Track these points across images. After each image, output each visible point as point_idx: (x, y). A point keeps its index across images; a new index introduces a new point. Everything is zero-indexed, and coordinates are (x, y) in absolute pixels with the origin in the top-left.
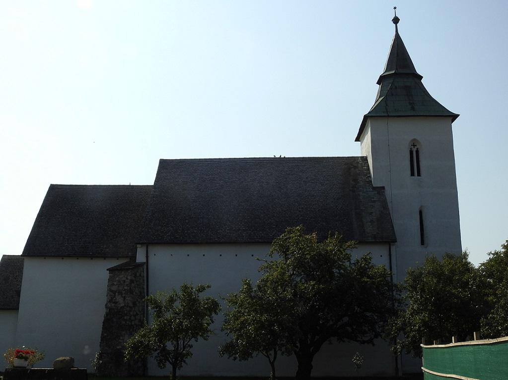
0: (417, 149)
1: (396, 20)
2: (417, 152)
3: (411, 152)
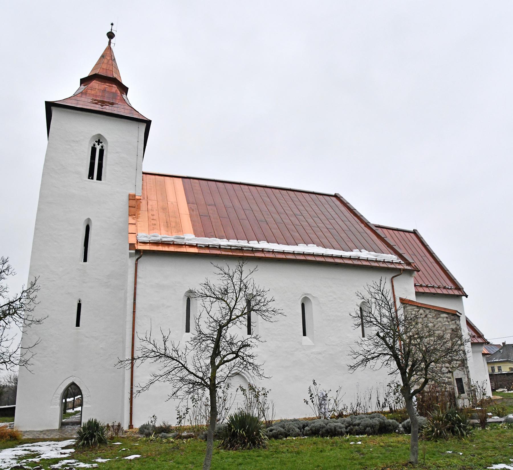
0: (102, 147)
1: (111, 35)
2: (102, 151)
3: (94, 150)
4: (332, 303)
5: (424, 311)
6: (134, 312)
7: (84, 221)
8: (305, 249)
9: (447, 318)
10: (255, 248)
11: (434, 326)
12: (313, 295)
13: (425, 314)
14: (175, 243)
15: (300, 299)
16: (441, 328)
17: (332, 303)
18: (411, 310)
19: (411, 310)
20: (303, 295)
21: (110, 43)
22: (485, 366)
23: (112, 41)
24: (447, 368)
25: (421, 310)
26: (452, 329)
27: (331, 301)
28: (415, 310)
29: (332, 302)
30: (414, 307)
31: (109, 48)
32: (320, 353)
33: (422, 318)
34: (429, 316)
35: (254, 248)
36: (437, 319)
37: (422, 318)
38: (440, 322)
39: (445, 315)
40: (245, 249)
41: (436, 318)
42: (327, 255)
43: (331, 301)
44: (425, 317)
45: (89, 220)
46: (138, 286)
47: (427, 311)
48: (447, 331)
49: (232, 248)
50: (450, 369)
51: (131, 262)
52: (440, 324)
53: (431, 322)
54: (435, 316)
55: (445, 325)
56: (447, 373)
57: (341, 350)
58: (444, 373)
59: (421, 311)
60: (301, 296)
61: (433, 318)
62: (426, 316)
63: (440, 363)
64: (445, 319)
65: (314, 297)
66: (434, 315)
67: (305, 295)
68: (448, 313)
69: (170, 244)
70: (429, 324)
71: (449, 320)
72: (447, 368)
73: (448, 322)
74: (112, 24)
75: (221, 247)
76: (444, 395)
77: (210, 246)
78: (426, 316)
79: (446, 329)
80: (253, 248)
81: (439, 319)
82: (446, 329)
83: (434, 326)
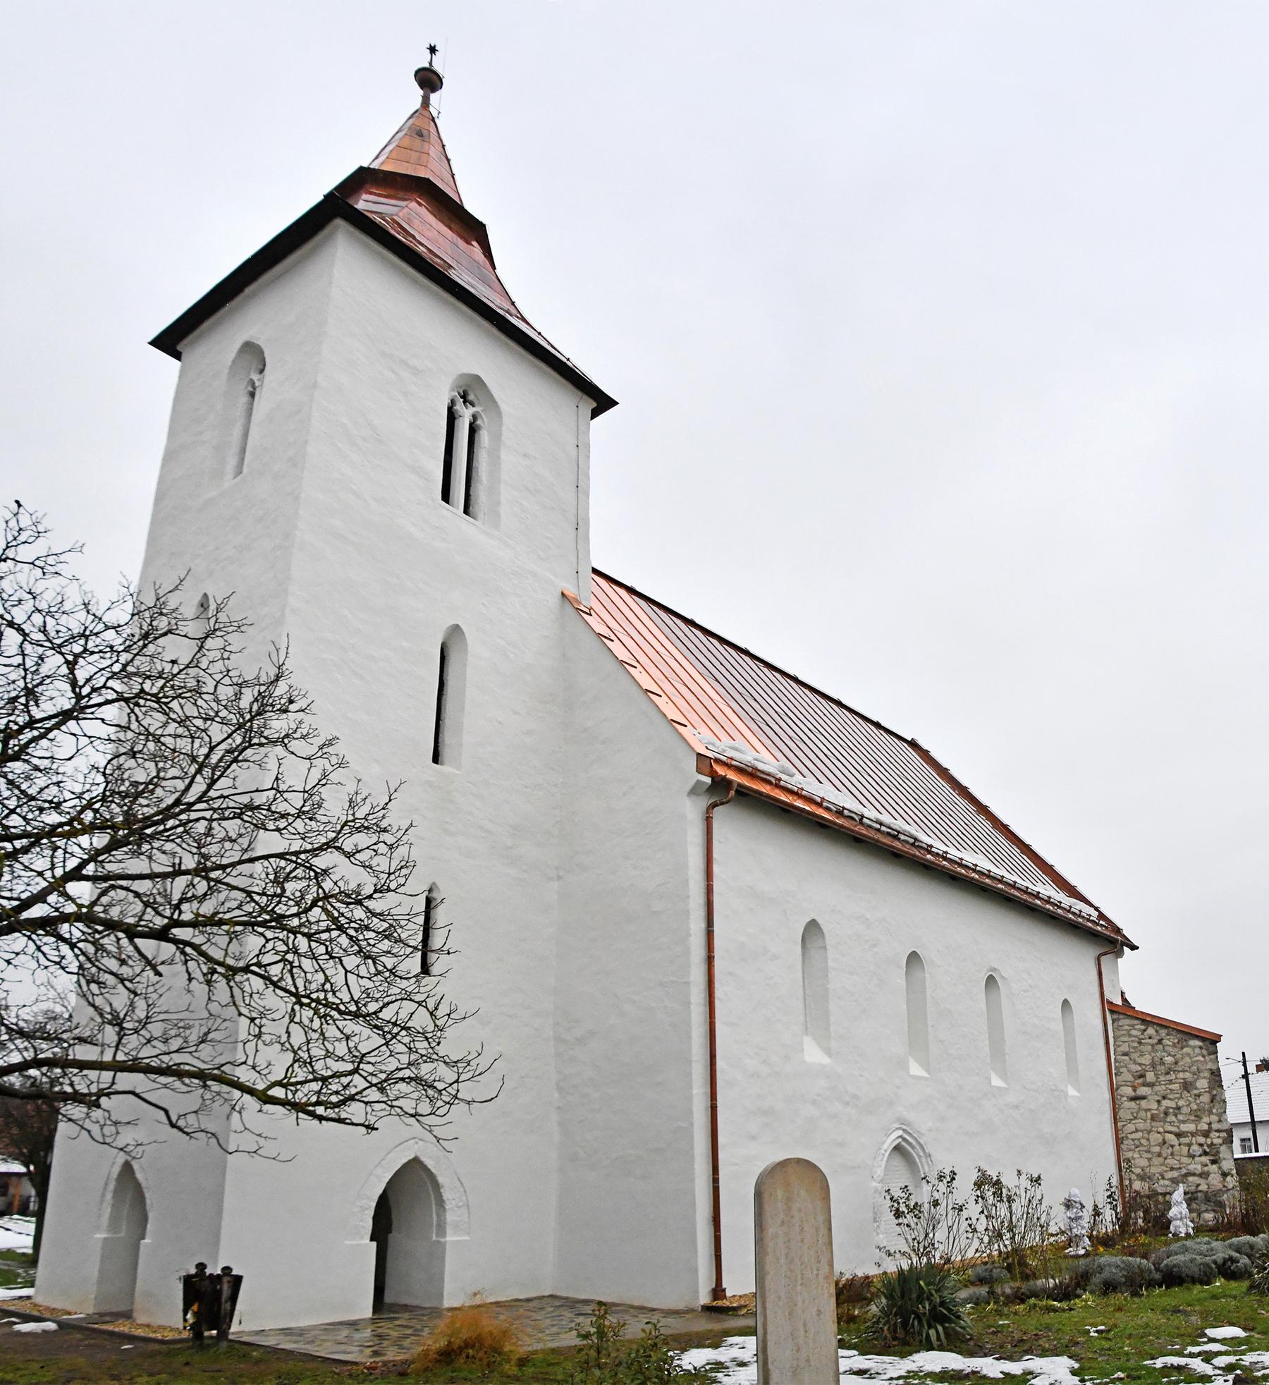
5: (1157, 1031)
6: (710, 960)
7: (448, 625)
9: (1201, 1048)
11: (1176, 1063)
12: (1004, 975)
13: (1158, 1038)
14: (782, 783)
16: (1190, 1068)
18: (1128, 1028)
19: (1128, 1028)
21: (426, 103)
22: (105, 1189)
24: (1201, 1145)
25: (1150, 1028)
26: (1211, 1070)
28: (1137, 1027)
30: (1136, 1022)
33: (1153, 1046)
34: (1166, 1042)
36: (1182, 1048)
37: (1153, 1046)
38: (1188, 1055)
39: (1197, 1043)
40: (902, 837)
41: (1180, 1046)
44: (1157, 1044)
45: (456, 630)
47: (1163, 1032)
48: (1202, 1075)
49: (883, 828)
50: (1206, 1148)
51: (693, 810)
52: (1187, 1059)
53: (1169, 1055)
54: (1178, 1043)
55: (1197, 1061)
56: (1200, 1156)
58: (1193, 1157)
59: (1151, 1031)
61: (1174, 1045)
62: (1160, 1042)
63: (1188, 1137)
64: (1197, 1051)
65: (1003, 977)
66: (1176, 1041)
67: (992, 971)
68: (1203, 1039)
70: (1166, 1058)
71: (1205, 1052)
72: (1201, 1145)
73: (1204, 1056)
75: (865, 820)
76: (1196, 1199)
77: (846, 812)
78: (1160, 1042)
79: (1199, 1071)
80: (916, 839)
81: (1185, 1050)
82: (1199, 1071)
83: (1176, 1063)
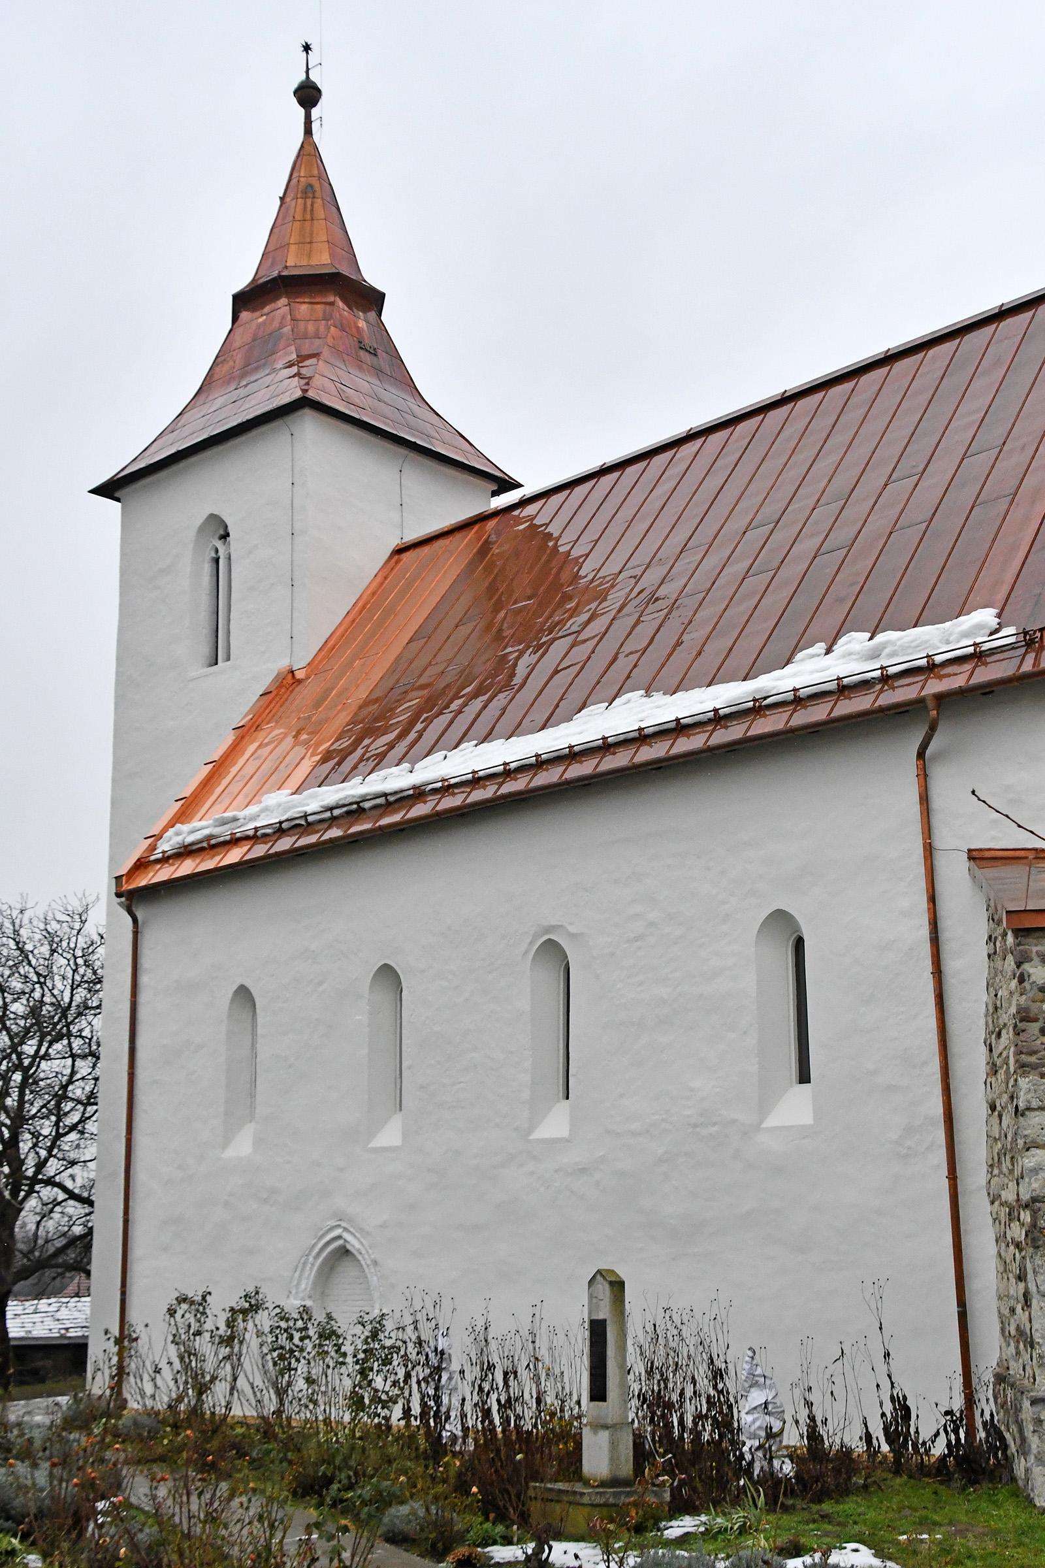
1: (308, 95)
4: (639, 948)
8: (343, 789)
10: (396, 793)
15: (526, 952)
17: (639, 948)
20: (536, 936)
23: (315, 112)
27: (637, 939)
29: (638, 944)
31: (308, 154)
32: (583, 1170)
35: (391, 794)
40: (367, 805)
42: (622, 737)
43: (637, 939)
46: (143, 999)
49: (336, 812)
57: (661, 1151)
60: (531, 943)
65: (573, 936)
69: (202, 849)
74: (307, 48)
77: (284, 826)
80: (385, 795)
